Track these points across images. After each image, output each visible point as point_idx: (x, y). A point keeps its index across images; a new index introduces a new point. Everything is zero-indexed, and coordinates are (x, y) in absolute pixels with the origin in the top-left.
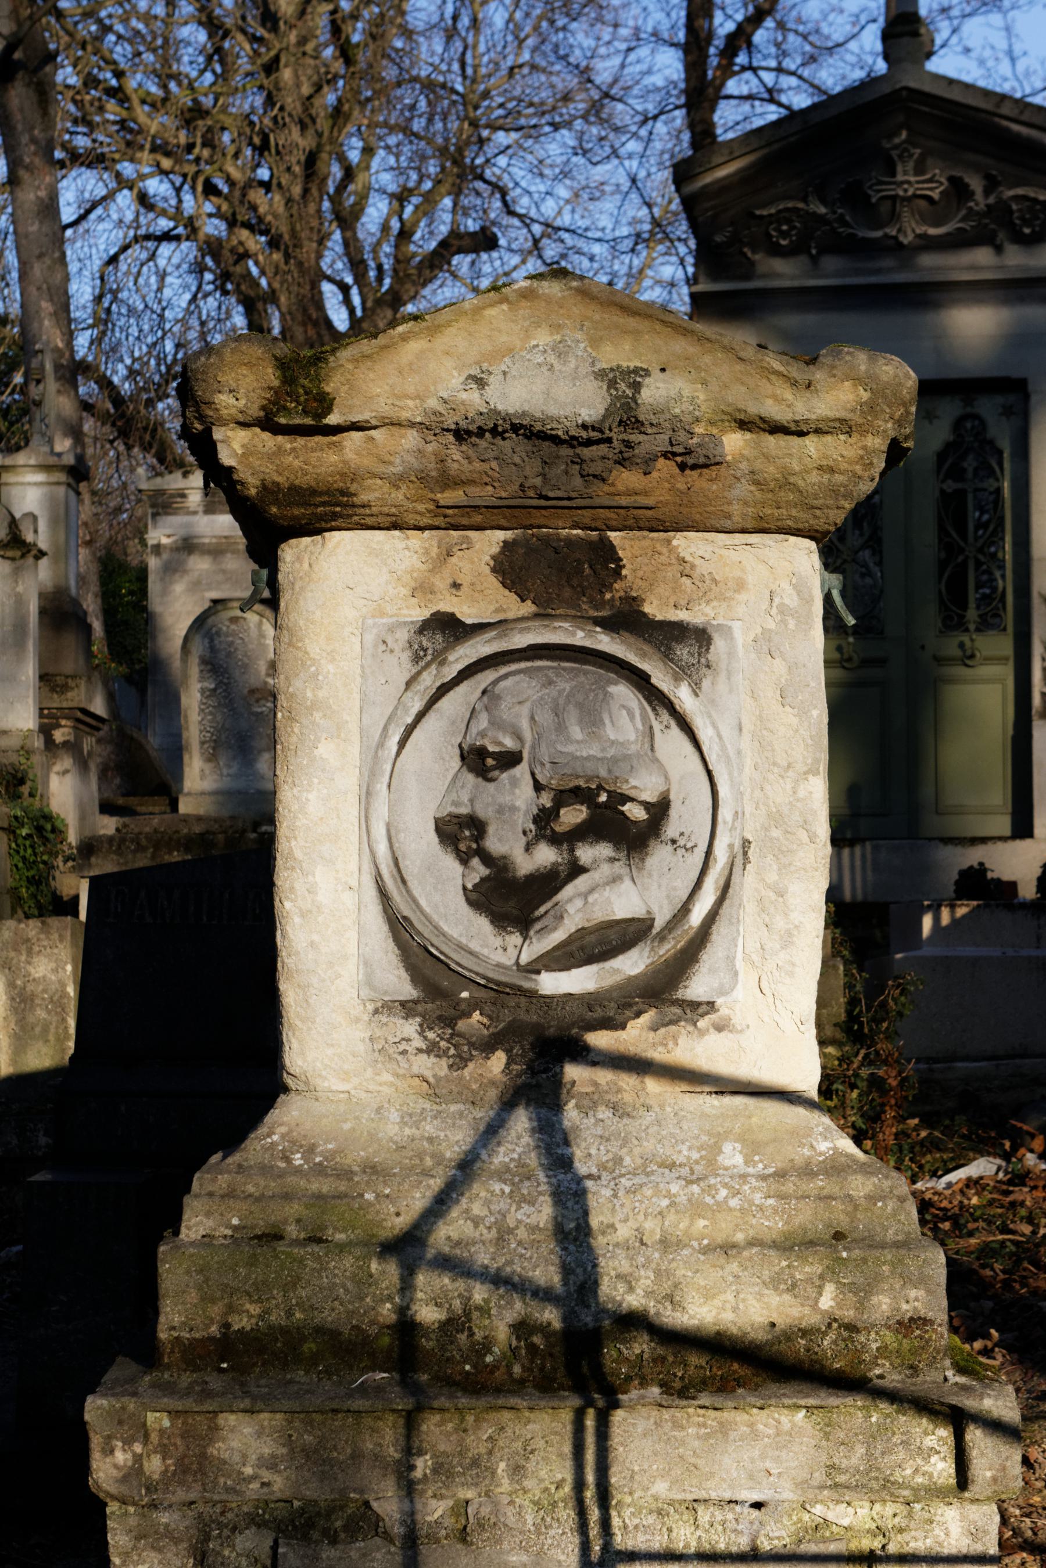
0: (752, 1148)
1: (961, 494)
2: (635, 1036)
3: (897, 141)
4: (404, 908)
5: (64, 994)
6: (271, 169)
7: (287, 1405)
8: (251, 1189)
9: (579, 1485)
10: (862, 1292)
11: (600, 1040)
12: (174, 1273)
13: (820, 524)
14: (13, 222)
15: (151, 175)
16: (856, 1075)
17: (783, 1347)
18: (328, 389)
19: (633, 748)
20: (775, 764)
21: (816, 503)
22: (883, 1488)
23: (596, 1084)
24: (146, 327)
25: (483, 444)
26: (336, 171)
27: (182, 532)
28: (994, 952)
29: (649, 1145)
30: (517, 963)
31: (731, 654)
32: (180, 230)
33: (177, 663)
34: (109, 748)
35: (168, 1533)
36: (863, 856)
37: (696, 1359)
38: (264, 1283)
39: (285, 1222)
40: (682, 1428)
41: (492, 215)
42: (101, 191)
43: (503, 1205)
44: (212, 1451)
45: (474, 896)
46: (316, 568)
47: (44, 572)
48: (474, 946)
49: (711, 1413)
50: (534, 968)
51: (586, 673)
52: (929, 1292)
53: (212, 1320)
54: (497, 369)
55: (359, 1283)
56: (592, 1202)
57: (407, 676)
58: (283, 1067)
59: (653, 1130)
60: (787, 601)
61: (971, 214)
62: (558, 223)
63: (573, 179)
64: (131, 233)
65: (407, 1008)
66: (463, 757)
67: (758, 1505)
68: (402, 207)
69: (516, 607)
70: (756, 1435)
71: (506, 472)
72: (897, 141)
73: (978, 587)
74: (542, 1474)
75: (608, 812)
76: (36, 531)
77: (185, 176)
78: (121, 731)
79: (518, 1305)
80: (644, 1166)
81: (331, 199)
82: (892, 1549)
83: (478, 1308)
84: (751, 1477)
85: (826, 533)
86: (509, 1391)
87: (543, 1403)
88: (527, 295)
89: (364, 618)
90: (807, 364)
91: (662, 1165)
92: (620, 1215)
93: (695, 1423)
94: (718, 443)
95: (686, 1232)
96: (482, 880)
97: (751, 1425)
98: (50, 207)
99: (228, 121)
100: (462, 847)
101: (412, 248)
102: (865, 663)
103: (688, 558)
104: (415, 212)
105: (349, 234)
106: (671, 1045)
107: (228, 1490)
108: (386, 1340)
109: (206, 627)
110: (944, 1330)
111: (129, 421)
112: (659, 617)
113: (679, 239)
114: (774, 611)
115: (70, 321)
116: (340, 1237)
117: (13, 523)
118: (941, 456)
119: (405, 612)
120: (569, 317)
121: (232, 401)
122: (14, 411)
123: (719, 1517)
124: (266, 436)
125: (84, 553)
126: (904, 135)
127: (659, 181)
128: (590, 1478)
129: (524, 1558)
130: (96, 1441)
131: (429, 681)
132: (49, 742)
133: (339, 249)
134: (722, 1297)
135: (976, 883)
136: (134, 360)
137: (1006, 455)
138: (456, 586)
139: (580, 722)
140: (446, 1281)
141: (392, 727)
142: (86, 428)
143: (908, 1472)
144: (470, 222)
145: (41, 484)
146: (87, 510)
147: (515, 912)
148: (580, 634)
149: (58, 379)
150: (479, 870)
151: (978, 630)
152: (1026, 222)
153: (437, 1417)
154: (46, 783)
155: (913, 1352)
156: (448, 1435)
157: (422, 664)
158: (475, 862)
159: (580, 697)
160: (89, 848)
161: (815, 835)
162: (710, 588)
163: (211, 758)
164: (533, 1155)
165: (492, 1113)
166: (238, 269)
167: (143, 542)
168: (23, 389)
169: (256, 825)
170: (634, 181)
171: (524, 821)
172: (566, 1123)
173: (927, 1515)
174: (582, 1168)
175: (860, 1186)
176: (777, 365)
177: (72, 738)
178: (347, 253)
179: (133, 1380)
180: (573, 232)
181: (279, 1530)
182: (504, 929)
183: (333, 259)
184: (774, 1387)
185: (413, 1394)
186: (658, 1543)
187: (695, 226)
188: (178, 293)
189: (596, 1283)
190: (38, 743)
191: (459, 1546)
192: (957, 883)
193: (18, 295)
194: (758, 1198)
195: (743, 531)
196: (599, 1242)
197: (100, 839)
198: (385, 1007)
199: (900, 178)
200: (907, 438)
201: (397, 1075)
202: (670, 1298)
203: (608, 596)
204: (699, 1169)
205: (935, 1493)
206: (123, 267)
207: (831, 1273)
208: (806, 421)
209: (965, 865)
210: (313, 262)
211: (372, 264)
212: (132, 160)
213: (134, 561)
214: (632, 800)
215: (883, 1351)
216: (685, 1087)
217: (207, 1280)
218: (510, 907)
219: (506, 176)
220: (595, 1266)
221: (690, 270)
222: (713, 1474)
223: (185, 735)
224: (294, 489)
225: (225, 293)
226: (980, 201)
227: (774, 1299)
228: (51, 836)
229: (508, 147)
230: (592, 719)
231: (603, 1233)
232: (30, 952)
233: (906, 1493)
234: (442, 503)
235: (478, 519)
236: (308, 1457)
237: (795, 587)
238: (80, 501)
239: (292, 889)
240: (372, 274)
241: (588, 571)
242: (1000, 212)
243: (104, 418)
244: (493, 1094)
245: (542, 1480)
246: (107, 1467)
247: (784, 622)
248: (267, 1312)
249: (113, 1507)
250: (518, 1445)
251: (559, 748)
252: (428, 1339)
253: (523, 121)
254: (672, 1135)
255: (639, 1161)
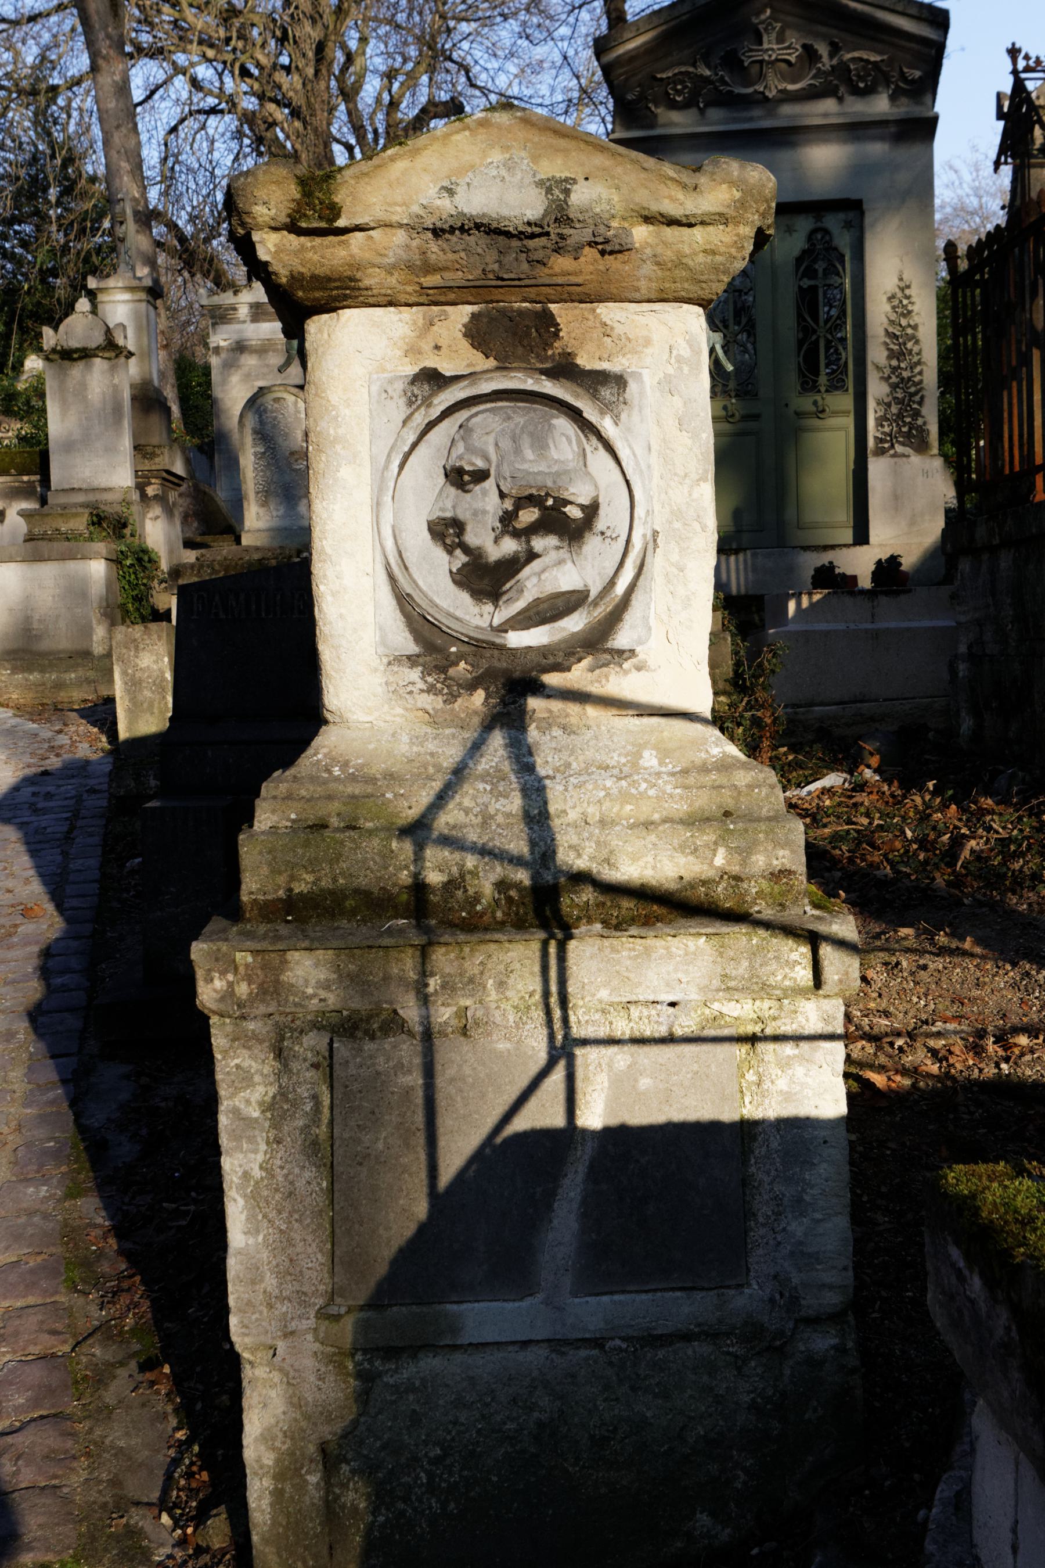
0: (664, 753)
1: (814, 289)
2: (578, 675)
3: (763, 17)
4: (407, 587)
5: (164, 679)
6: (290, 56)
7: (335, 944)
8: (303, 793)
9: (546, 994)
10: (745, 853)
11: (552, 679)
12: (252, 855)
13: (706, 294)
14: (97, 102)
15: (199, 63)
16: (741, 716)
17: (689, 893)
18: (337, 199)
19: (571, 465)
20: (675, 474)
21: (703, 278)
22: (762, 989)
23: (550, 711)
24: (201, 182)
25: (454, 239)
26: (340, 57)
27: (235, 337)
28: (841, 626)
29: (590, 754)
30: (491, 625)
31: (642, 393)
32: (223, 105)
33: (236, 436)
34: (189, 500)
35: (255, 1036)
36: (745, 561)
37: (627, 904)
38: (316, 859)
39: (329, 815)
40: (618, 952)
41: (459, 88)
42: (161, 76)
43: (486, 799)
44: (282, 977)
45: (458, 577)
46: (333, 337)
47: (133, 369)
48: (459, 613)
49: (638, 940)
50: (503, 629)
51: (535, 410)
52: (793, 852)
53: (279, 887)
54: (462, 182)
55: (384, 857)
56: (550, 795)
57: (403, 416)
58: (323, 706)
59: (592, 743)
60: (682, 353)
61: (819, 73)
62: (510, 93)
63: (518, 57)
64: (187, 109)
65: (412, 660)
66: (446, 475)
67: (673, 1004)
68: (391, 84)
69: (482, 363)
70: (670, 956)
71: (472, 260)
72: (763, 17)
73: (827, 366)
74: (520, 986)
75: (554, 513)
76: (125, 337)
77: (225, 63)
78: (196, 487)
79: (499, 869)
80: (587, 768)
81: (337, 79)
82: (769, 1031)
83: (470, 872)
84: (668, 985)
85: (710, 301)
86: (494, 930)
87: (518, 937)
88: (483, 123)
89: (370, 374)
90: (694, 171)
91: (599, 767)
92: (570, 804)
93: (626, 948)
94: (628, 233)
95: (617, 814)
96: (464, 565)
97: (667, 948)
98: (123, 88)
99: (256, 19)
100: (448, 541)
101: (400, 115)
102: (745, 418)
103: (608, 322)
104: (400, 88)
105: (351, 106)
106: (604, 681)
107: (296, 1005)
108: (404, 897)
109: (256, 406)
110: (804, 878)
111: (192, 254)
112: (588, 368)
113: (601, 103)
114: (673, 361)
115: (143, 178)
116: (369, 825)
117: (108, 331)
118: (799, 260)
119: (400, 368)
120: (515, 140)
121: (266, 211)
122: (105, 249)
123: (645, 1013)
124: (292, 237)
125: (162, 354)
126: (768, 12)
127: (585, 58)
128: (554, 988)
129: (508, 1045)
130: (200, 974)
131: (420, 419)
132: (143, 496)
133: (345, 118)
134: (645, 859)
135: (827, 578)
136: (193, 208)
137: (847, 258)
138: (437, 347)
139: (532, 446)
140: (447, 853)
141: (393, 454)
142: (159, 261)
143: (779, 978)
144: (442, 93)
145: (128, 301)
146: (163, 323)
147: (489, 588)
148: (530, 381)
149: (136, 221)
150: (461, 558)
151: (827, 391)
152: (861, 78)
153: (443, 950)
154: (143, 527)
155: (782, 894)
156: (452, 961)
157: (414, 407)
158: (458, 552)
159: (531, 428)
160: (176, 572)
161: (706, 526)
162: (626, 345)
163: (264, 504)
164: (506, 763)
165: (476, 735)
166: (268, 135)
167: (206, 345)
168: (111, 232)
169: (299, 552)
170: (565, 58)
171: (492, 520)
172: (530, 740)
173: (793, 1008)
174: (542, 771)
175: (742, 778)
176: (671, 173)
177: (160, 492)
178: (351, 121)
179: (224, 930)
180: (521, 99)
181: (333, 1032)
182: (480, 601)
183: (340, 126)
184: (683, 921)
185: (426, 933)
186: (602, 1032)
187: (612, 91)
188: (224, 156)
189: (554, 852)
190: (135, 496)
191: (462, 1039)
192: (813, 577)
193: (103, 160)
194: (669, 789)
195: (649, 301)
196: (556, 823)
197: (184, 566)
198: (396, 660)
199: (765, 46)
200: (769, 227)
201: (407, 709)
202: (607, 861)
203: (550, 352)
204: (626, 769)
205: (799, 992)
206: (182, 135)
207: (722, 839)
208: (694, 216)
209: (819, 564)
210: (325, 127)
211: (369, 128)
212: (184, 51)
213: (199, 361)
214: (571, 503)
215: (760, 894)
216: (615, 712)
217: (274, 858)
218: (485, 584)
219: (469, 57)
220: (553, 840)
221: (610, 127)
222: (640, 984)
223: (244, 487)
224: (314, 277)
225: (260, 154)
226: (826, 62)
227: (682, 860)
228: (148, 565)
229: (470, 34)
230: (541, 443)
231: (558, 817)
232: (137, 648)
233: (778, 992)
234: (425, 285)
235: (452, 296)
236: (352, 980)
237: (688, 342)
238: (158, 315)
239: (325, 576)
240: (370, 136)
241: (534, 334)
242: (842, 71)
243: (171, 252)
244: (476, 721)
245: (519, 991)
246: (209, 992)
247: (680, 369)
248: (319, 879)
249: (214, 1020)
250: (502, 967)
251: (517, 466)
252: (435, 895)
253: (480, 14)
254: (606, 746)
255: (583, 765)
